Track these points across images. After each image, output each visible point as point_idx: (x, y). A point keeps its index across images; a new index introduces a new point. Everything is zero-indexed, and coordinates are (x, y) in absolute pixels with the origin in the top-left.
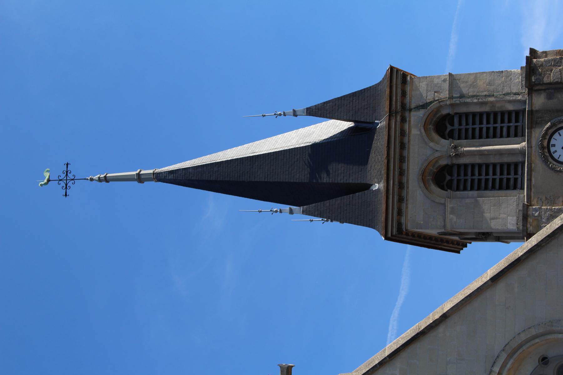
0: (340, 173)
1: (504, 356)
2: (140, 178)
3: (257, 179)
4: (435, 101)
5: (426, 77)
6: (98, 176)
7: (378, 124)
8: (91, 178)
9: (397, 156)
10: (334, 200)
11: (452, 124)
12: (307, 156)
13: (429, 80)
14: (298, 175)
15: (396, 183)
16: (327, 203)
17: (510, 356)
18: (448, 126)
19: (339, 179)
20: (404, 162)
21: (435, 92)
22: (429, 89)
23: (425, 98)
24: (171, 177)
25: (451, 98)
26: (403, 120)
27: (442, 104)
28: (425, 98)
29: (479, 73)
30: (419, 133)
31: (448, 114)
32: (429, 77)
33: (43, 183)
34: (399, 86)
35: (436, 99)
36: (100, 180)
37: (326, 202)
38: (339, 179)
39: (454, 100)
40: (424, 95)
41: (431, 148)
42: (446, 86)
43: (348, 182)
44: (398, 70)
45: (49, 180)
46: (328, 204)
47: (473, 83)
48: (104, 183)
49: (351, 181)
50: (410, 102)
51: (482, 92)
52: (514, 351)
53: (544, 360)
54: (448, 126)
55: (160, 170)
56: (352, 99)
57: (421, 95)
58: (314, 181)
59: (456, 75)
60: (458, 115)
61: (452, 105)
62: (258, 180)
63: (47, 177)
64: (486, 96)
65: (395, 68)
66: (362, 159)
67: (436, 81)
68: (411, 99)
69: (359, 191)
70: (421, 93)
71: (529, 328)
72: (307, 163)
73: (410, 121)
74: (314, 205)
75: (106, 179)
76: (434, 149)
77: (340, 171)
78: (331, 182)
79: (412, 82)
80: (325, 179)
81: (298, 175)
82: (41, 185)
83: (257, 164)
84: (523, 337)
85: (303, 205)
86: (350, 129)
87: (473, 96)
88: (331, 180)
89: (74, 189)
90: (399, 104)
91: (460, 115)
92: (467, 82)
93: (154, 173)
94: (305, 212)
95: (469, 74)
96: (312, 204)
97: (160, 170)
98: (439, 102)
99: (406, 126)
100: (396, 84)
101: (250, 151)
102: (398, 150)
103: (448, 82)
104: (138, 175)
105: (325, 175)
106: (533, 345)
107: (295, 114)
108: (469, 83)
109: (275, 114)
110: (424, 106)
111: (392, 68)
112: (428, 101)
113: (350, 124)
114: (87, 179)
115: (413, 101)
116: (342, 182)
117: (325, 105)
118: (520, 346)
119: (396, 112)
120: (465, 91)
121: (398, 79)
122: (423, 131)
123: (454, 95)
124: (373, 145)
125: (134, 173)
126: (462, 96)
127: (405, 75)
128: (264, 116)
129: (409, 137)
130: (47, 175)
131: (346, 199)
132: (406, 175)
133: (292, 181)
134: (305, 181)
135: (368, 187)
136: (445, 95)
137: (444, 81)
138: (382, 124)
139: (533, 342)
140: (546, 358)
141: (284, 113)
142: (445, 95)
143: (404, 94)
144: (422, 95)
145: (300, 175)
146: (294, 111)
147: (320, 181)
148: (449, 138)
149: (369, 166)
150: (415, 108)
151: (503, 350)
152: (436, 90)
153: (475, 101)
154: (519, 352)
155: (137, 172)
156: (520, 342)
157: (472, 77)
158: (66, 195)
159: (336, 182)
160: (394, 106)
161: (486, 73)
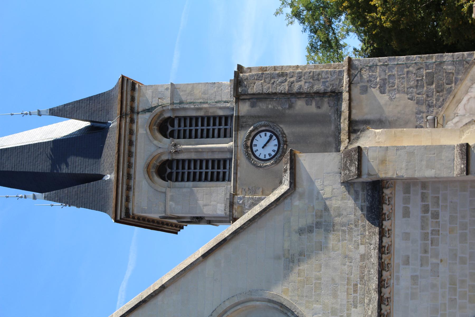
0: (77, 165)
5: (152, 86)
11: (173, 126)
12: (49, 150)
13: (155, 88)
14: (41, 166)
16: (66, 190)
18: (169, 126)
20: (132, 156)
21: (159, 98)
23: (150, 103)
25: (172, 103)
26: (132, 121)
27: (164, 108)
28: (150, 103)
30: (145, 132)
34: (129, 93)
35: (160, 104)
37: (64, 189)
39: (175, 105)
40: (150, 101)
41: (155, 145)
42: (168, 93)
43: (84, 173)
44: (128, 79)
46: (66, 192)
47: (191, 91)
49: (86, 172)
50: (138, 107)
51: (198, 99)
54: (169, 126)
56: (88, 102)
57: (147, 100)
58: (55, 172)
59: (177, 84)
61: (173, 110)
64: (201, 103)
65: (125, 77)
66: (97, 153)
67: (160, 89)
68: (138, 104)
71: (233, 297)
72: (49, 155)
73: (137, 122)
74: (54, 192)
77: (77, 164)
78: (69, 172)
79: (140, 89)
80: (64, 170)
81: (41, 166)
84: (228, 304)
86: (87, 128)
87: (190, 103)
88: (69, 170)
91: (180, 118)
92: (185, 91)
98: (163, 107)
99: (134, 127)
103: (170, 90)
105: (65, 167)
106: (236, 310)
107: (39, 114)
108: (188, 92)
109: (22, 114)
110: (149, 110)
111: (123, 77)
112: (153, 106)
115: (140, 105)
116: (79, 172)
117: (66, 107)
118: (225, 312)
119: (126, 115)
120: (184, 98)
121: (128, 86)
122: (148, 130)
123: (175, 102)
124: (106, 142)
126: (181, 103)
127: (134, 84)
128: (12, 115)
129: (137, 135)
131: (83, 187)
132: (133, 168)
134: (48, 171)
135: (100, 177)
136: (167, 101)
137: (167, 89)
141: (30, 112)
142: (167, 101)
143: (133, 99)
145: (43, 166)
146: (39, 111)
148: (170, 137)
149: (102, 159)
150: (142, 111)
152: (160, 97)
153: (192, 107)
156: (225, 308)
159: (74, 172)
160: (124, 109)
161: (201, 83)
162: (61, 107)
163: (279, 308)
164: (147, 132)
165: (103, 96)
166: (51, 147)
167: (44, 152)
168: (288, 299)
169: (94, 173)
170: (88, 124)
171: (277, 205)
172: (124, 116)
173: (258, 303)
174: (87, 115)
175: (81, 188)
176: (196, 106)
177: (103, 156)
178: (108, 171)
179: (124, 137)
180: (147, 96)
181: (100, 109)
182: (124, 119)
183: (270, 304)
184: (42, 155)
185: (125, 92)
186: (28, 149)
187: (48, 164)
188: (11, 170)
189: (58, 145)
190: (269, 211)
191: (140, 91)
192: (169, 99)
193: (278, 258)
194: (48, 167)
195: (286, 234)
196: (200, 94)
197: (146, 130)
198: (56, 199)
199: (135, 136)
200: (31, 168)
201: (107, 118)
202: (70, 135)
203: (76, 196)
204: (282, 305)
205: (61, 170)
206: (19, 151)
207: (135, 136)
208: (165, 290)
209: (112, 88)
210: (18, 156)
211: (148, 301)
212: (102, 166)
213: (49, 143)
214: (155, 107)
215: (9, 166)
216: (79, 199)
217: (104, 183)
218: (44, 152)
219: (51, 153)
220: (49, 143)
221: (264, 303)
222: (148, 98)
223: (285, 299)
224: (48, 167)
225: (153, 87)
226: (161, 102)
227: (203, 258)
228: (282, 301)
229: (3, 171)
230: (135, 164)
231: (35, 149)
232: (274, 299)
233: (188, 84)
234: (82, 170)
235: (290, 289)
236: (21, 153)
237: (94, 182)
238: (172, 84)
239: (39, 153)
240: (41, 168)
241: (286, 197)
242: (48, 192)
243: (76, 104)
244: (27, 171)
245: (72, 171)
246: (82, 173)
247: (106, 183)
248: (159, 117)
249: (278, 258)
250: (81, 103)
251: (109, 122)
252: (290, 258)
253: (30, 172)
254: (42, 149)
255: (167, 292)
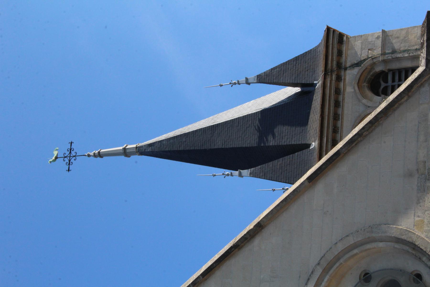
0: (284, 135)
1: (319, 271)
2: (126, 153)
3: (216, 147)
4: (369, 58)
5: (361, 36)
6: (94, 152)
7: (316, 84)
8: (88, 154)
9: (332, 114)
10: (276, 161)
11: (386, 81)
12: (257, 122)
14: (249, 140)
15: (330, 140)
16: (270, 164)
17: (326, 271)
19: (283, 141)
20: (338, 119)
21: (369, 50)
22: (364, 47)
23: (359, 56)
24: (149, 149)
25: (383, 54)
26: (339, 79)
27: (375, 60)
28: (359, 56)
29: (411, 27)
30: (353, 90)
31: (382, 72)
32: (364, 35)
33: (51, 160)
34: (336, 46)
35: (370, 56)
36: (95, 155)
37: (269, 163)
38: (283, 141)
39: (387, 56)
40: (359, 53)
43: (290, 144)
44: (334, 31)
45: (56, 158)
46: (271, 165)
47: (405, 37)
48: (99, 158)
49: (293, 143)
50: (346, 62)
51: (413, 46)
52: (330, 265)
53: (366, 277)
55: (142, 144)
56: (295, 63)
57: (356, 53)
58: (262, 145)
59: (389, 31)
60: (391, 72)
62: (217, 147)
63: (55, 155)
64: (416, 49)
65: (332, 28)
66: (303, 121)
67: (370, 39)
68: (346, 58)
69: (298, 151)
70: (356, 52)
71: (347, 236)
72: (257, 128)
73: (345, 79)
74: (259, 167)
75: (100, 155)
76: (366, 106)
77: (284, 134)
78: (276, 144)
79: (348, 41)
80: (272, 142)
81: (249, 140)
82: (51, 162)
83: (216, 132)
84: (341, 247)
85: (250, 168)
86: (297, 94)
87: (404, 51)
88: (276, 142)
89: (76, 164)
90: (335, 63)
91: (393, 72)
92: (398, 37)
93: (136, 147)
94: (253, 175)
95: (401, 30)
96: (258, 166)
97: (142, 144)
98: (373, 59)
100: (332, 44)
101: (213, 121)
102: (332, 108)
103: (381, 39)
104: (125, 149)
105: (272, 138)
107: (248, 82)
108: (401, 38)
109: (230, 83)
110: (358, 64)
111: (328, 29)
112: (362, 59)
113: (298, 90)
114: (86, 155)
115: (348, 59)
116: (285, 144)
117: (273, 71)
118: (337, 258)
119: (332, 71)
120: (397, 46)
121: (334, 39)
122: (356, 88)
124: (313, 106)
125: (121, 148)
126: (394, 52)
127: (341, 36)
128: (221, 86)
129: (344, 95)
130: (55, 153)
132: (339, 132)
133: (244, 146)
134: (255, 145)
135: (309, 146)
137: (378, 38)
138: (319, 84)
139: (351, 254)
140: (366, 274)
141: (238, 81)
142: (378, 52)
143: (340, 53)
144: (357, 54)
145: (250, 140)
146: (247, 79)
147: (267, 145)
148: (383, 94)
149: (309, 126)
150: (350, 67)
151: (319, 264)
152: (370, 47)
153: (406, 55)
154: (335, 267)
155: (124, 147)
156: (336, 253)
157: (404, 32)
158: (69, 170)
159: (281, 144)
161: (417, 27)
162: (268, 72)
163: (410, 250)
164: (355, 90)
165: (310, 54)
166: (259, 118)
167: (252, 124)
168: (423, 236)
169: (300, 143)
170: (298, 90)
171: (409, 97)
172: (329, 73)
173: (381, 244)
174: (294, 78)
175: (286, 161)
176: (411, 55)
177: (309, 123)
178: (313, 139)
179: (329, 97)
180: (356, 48)
181: (307, 69)
182: (330, 76)
183: (397, 246)
184: (250, 127)
185: (331, 46)
186: (237, 123)
187: (256, 137)
188: (221, 147)
189: (266, 114)
190: (397, 108)
191: (348, 44)
192: (380, 49)
193: (410, 175)
194: (256, 141)
195: (422, 138)
196: (416, 39)
197: (354, 88)
198: (261, 174)
199: (342, 96)
200: (240, 142)
201: (313, 79)
202: (279, 103)
203: (281, 170)
204: (414, 246)
205: (268, 143)
206: (229, 126)
207: (342, 96)
208: (263, 230)
209: (318, 44)
210: (229, 131)
211: (243, 246)
212: (308, 134)
213: (258, 114)
214: (365, 60)
215: (219, 143)
216: (283, 173)
217: (309, 153)
218: (252, 124)
219: (259, 125)
220: (258, 114)
221: (389, 244)
222: (358, 51)
223: (418, 237)
224: (256, 141)
225: (363, 37)
226: (371, 54)
227: (309, 182)
228: (414, 239)
229: (214, 149)
230: (342, 128)
231: (244, 122)
232: (403, 237)
233: (401, 29)
234: (288, 141)
235: (426, 221)
236: (231, 127)
237: (299, 153)
238: (383, 31)
239: (248, 126)
240: (249, 142)
241: (422, 84)
242: (254, 167)
243: (282, 67)
244: (236, 146)
245: (278, 143)
246: (288, 144)
247: (311, 152)
248: (370, 71)
249: (410, 175)
250: (287, 65)
251: (315, 82)
252: (426, 173)
253: (239, 147)
254: (251, 121)
255: (266, 232)
